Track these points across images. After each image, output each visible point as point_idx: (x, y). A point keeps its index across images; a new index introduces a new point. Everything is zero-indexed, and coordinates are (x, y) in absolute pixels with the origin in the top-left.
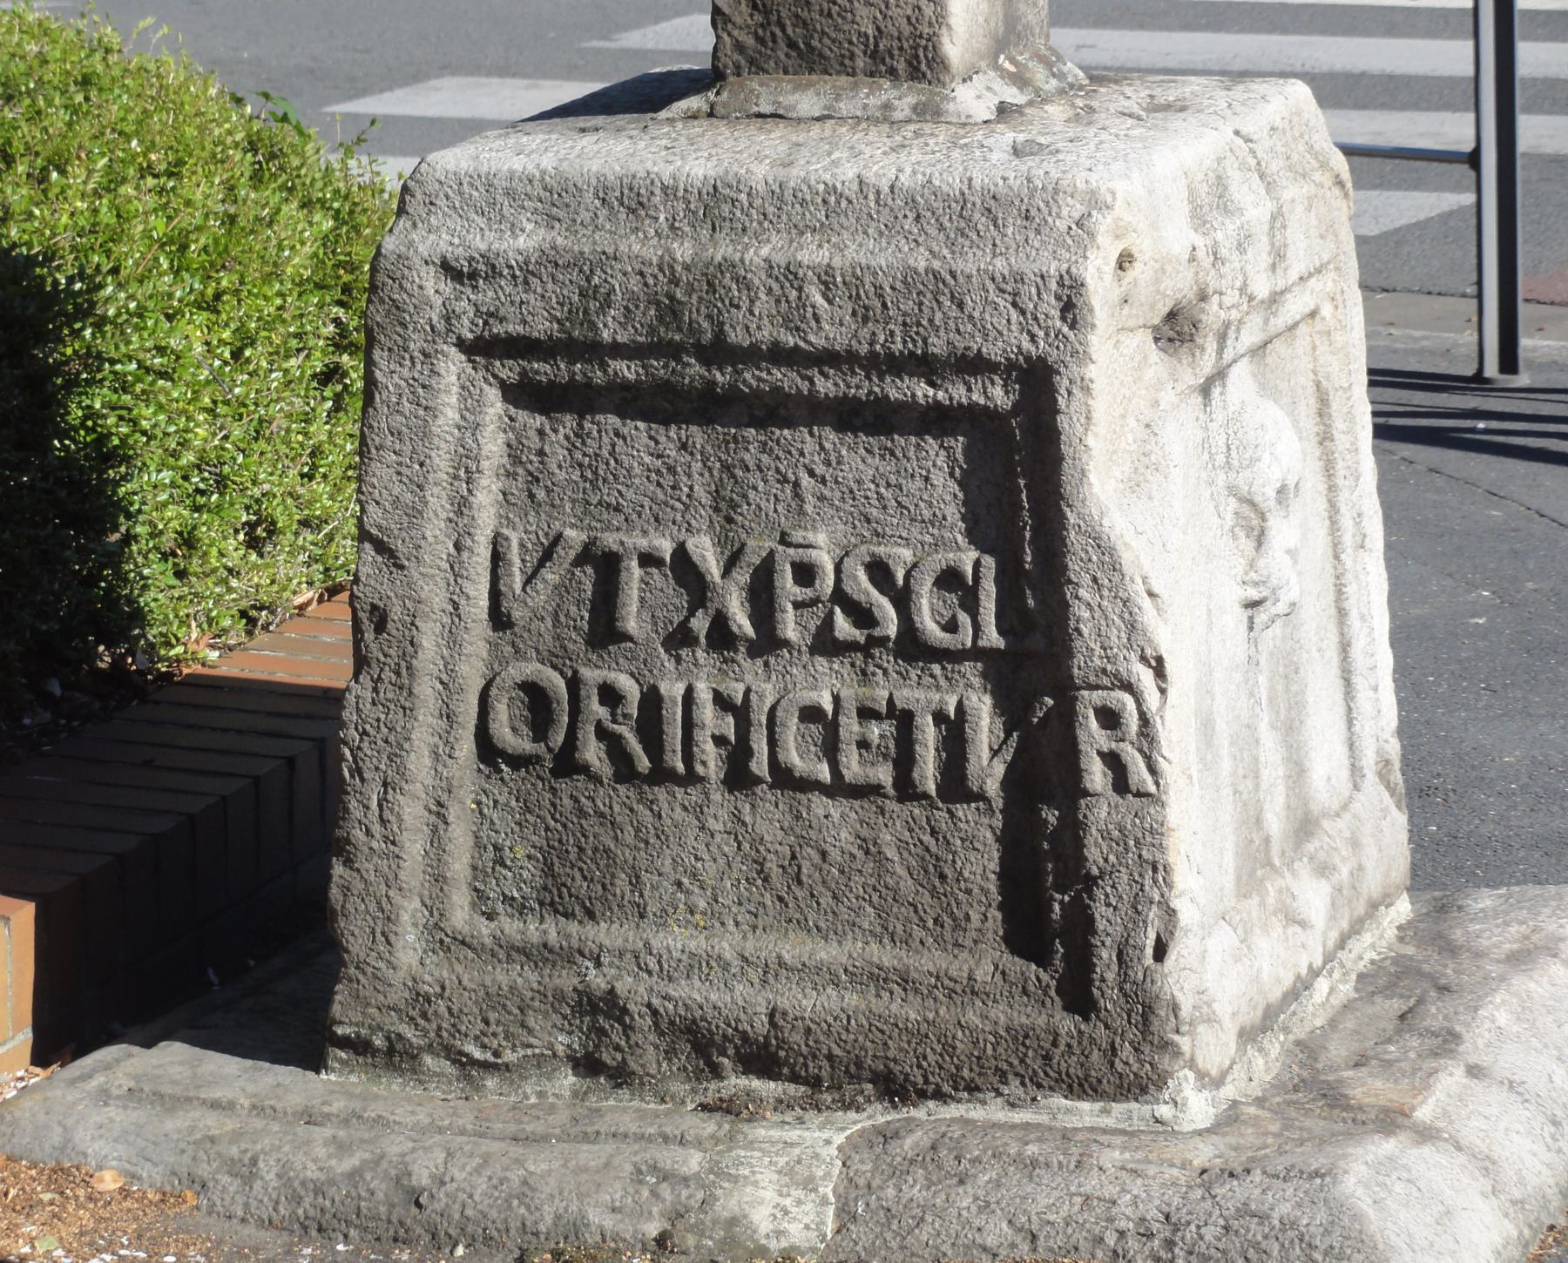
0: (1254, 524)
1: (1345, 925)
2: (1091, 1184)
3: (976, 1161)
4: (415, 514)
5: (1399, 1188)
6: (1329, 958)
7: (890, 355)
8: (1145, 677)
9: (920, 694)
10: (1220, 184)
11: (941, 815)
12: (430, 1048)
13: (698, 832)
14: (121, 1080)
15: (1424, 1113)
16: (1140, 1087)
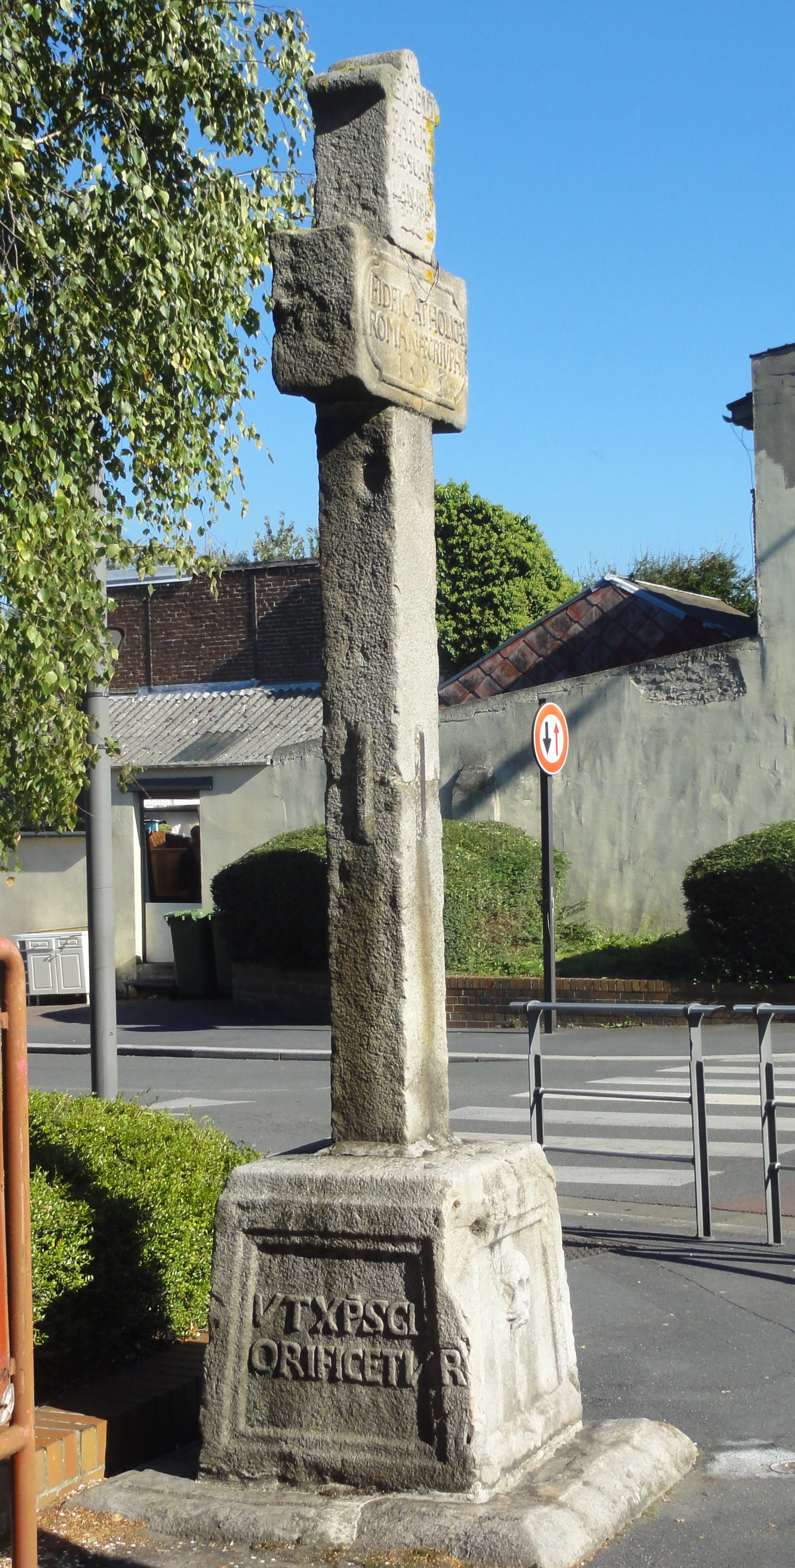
0: (511, 1293)
1: (552, 1432)
2: (442, 1521)
3: (405, 1513)
4: (228, 1288)
5: (545, 1524)
6: (544, 1443)
7: (380, 1235)
8: (463, 1345)
9: (391, 1350)
10: (498, 1178)
11: (398, 1392)
12: (231, 1472)
13: (320, 1398)
14: (127, 1483)
15: (562, 1498)
16: (463, 1488)
